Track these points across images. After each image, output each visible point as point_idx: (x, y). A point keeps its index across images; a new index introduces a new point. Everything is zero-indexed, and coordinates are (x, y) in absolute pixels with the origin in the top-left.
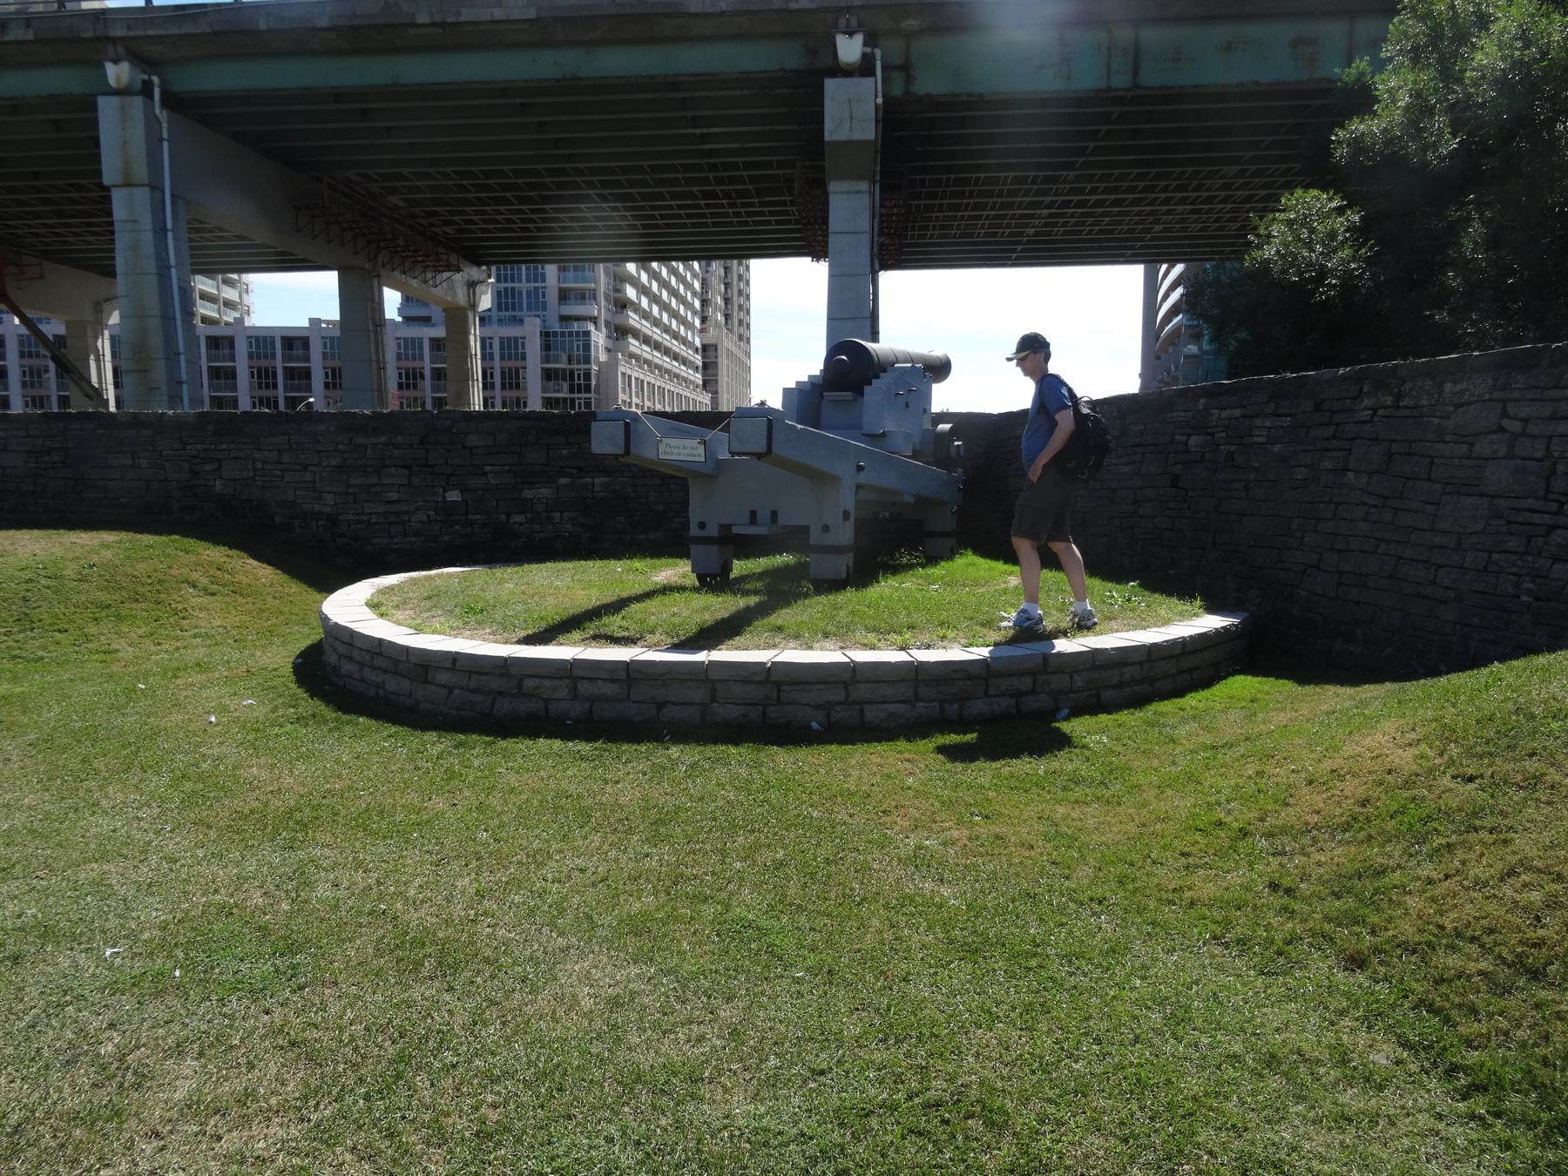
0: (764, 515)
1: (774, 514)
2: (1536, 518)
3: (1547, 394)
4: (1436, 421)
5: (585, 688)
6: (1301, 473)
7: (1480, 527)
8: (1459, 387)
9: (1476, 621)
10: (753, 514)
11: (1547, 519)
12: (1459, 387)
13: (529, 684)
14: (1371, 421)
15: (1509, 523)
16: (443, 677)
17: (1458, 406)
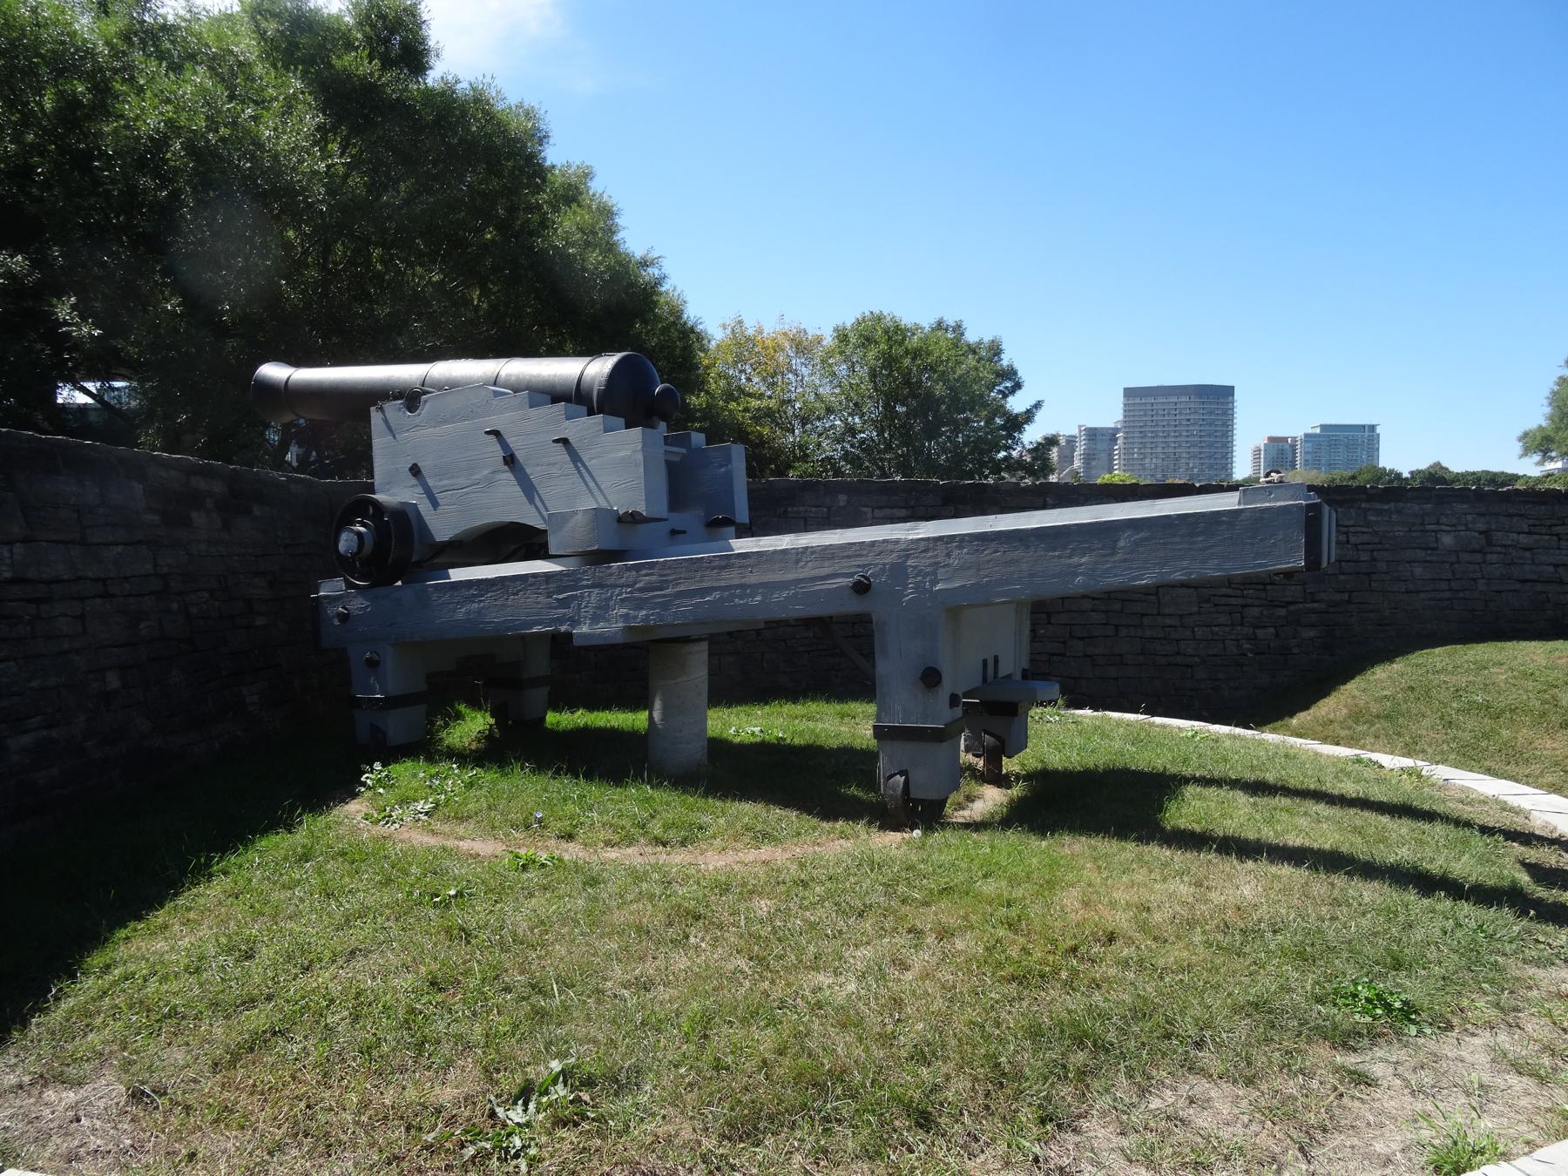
2: (1232, 601)
7: (1195, 609)
11: (1240, 601)
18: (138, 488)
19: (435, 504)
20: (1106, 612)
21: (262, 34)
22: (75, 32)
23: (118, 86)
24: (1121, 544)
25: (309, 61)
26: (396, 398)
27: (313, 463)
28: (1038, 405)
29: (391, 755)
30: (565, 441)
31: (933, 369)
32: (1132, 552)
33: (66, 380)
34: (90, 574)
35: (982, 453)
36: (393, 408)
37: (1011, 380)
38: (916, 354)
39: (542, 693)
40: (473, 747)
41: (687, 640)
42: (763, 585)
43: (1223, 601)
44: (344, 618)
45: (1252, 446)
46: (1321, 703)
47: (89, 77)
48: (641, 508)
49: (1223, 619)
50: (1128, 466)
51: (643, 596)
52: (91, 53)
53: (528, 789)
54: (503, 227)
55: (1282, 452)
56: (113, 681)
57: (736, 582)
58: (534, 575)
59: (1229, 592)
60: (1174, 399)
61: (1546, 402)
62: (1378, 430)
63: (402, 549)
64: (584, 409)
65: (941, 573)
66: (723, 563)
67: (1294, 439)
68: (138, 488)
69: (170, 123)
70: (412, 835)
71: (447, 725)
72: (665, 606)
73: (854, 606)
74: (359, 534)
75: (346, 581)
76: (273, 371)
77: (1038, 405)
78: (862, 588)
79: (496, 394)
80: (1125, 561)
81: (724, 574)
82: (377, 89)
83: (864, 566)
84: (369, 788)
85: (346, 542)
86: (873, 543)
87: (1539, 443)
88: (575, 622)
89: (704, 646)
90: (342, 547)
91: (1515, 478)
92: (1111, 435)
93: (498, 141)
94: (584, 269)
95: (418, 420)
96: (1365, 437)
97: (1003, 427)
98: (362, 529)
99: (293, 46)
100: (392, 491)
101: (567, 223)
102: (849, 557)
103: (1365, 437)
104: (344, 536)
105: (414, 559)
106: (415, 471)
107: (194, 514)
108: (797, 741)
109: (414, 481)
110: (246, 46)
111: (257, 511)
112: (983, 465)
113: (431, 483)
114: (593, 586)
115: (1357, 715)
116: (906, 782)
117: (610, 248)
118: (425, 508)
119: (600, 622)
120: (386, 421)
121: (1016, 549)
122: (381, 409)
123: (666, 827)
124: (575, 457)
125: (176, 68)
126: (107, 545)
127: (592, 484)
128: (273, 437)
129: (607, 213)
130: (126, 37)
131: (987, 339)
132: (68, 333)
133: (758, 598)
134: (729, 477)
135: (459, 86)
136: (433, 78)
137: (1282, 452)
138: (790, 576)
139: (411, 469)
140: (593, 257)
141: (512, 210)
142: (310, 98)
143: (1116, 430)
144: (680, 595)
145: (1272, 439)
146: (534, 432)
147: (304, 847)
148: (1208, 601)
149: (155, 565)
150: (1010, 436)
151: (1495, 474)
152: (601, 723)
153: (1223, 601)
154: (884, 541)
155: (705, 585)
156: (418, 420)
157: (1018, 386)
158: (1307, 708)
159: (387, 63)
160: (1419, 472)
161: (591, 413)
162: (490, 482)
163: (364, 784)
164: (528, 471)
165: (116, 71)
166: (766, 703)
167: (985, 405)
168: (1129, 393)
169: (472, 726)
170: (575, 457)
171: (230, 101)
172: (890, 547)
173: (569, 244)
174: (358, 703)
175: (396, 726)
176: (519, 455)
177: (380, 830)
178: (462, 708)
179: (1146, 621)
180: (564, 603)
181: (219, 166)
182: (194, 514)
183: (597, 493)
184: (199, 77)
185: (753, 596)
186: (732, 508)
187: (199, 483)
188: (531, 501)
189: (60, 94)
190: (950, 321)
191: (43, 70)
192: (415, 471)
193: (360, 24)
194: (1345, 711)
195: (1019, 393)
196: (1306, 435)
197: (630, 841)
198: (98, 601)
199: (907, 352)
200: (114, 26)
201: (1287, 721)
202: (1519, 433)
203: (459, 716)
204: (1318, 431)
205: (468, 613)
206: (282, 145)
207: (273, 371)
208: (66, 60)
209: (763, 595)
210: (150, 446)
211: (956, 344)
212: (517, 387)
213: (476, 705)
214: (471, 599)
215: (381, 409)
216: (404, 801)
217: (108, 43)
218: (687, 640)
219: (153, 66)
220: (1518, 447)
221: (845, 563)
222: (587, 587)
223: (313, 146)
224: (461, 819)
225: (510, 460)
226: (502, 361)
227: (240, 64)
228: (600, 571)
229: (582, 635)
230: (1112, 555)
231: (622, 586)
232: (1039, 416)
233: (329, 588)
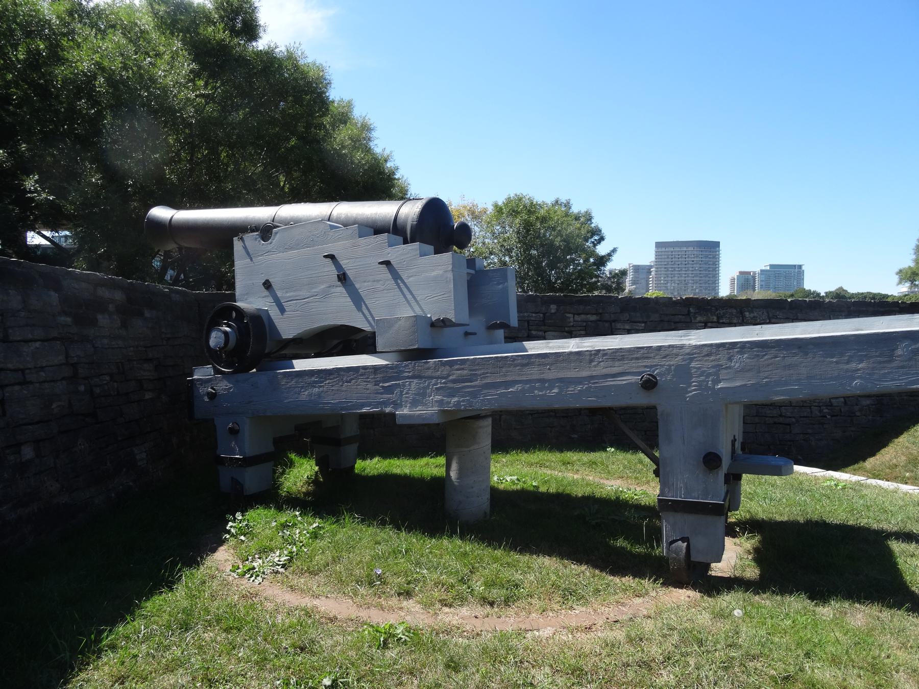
8: (752, 315)
9: (810, 431)
12: (752, 315)
18: (54, 297)
19: (282, 310)
21: (155, 14)
22: (39, 10)
23: (65, 43)
24: (899, 352)
25: (186, 30)
26: (253, 231)
27: (182, 280)
28: (614, 250)
29: (246, 503)
30: (387, 263)
31: (554, 229)
32: (910, 359)
33: (33, 230)
34: (10, 366)
35: (583, 279)
37: (597, 235)
38: (544, 220)
39: (352, 448)
40: (304, 490)
41: (478, 417)
42: (561, 380)
44: (212, 396)
45: (730, 277)
46: (883, 451)
47: (47, 39)
48: (451, 316)
50: (658, 287)
51: (456, 386)
52: (49, 23)
53: (364, 541)
54: (301, 138)
55: (747, 280)
56: (28, 452)
57: (535, 377)
58: (365, 368)
60: (685, 249)
61: (912, 252)
62: (803, 268)
63: (258, 346)
64: (401, 239)
65: (723, 374)
66: (525, 361)
67: (754, 273)
69: (97, 64)
70: (281, 597)
71: (283, 473)
72: (474, 395)
73: (642, 399)
74: (225, 333)
75: (214, 368)
76: (161, 213)
77: (614, 250)
78: (649, 384)
79: (332, 227)
80: (902, 367)
81: (526, 370)
82: (227, 51)
83: (651, 367)
84: (233, 535)
85: (215, 339)
87: (909, 276)
88: (397, 405)
89: (489, 421)
90: (213, 342)
91: (887, 296)
92: (647, 270)
93: (301, 82)
94: (352, 163)
95: (270, 247)
96: (796, 272)
97: (594, 264)
98: (228, 329)
99: (175, 22)
100: (250, 301)
101: (342, 135)
102: (637, 359)
103: (796, 272)
104: (214, 334)
105: (266, 351)
106: (267, 285)
107: (99, 317)
108: (543, 489)
109: (266, 293)
110: (146, 22)
111: (147, 314)
112: (583, 286)
113: (279, 294)
114: (413, 377)
115: (914, 462)
116: (688, 547)
117: (368, 150)
118: (274, 313)
119: (417, 407)
120: (245, 248)
121: (795, 354)
122: (242, 239)
123: (490, 584)
124: (396, 276)
125: (103, 33)
126: (27, 341)
127: (409, 296)
128: (157, 263)
129: (366, 128)
130: (71, 13)
131: (583, 210)
132: (32, 199)
133: (556, 390)
134: (505, 292)
135: (277, 50)
136: (261, 45)
137: (747, 280)
138: (585, 374)
139: (264, 284)
140: (359, 155)
141: (308, 126)
142: (186, 53)
143: (651, 267)
145: (741, 273)
146: (362, 257)
147: (184, 611)
149: (67, 357)
150: (598, 269)
151: (875, 294)
152: (397, 471)
154: (670, 346)
155: (509, 378)
156: (270, 247)
157: (602, 239)
158: (873, 454)
159: (235, 33)
160: (830, 292)
161: (405, 242)
162: (326, 294)
163: (229, 532)
164: (357, 286)
165: (64, 35)
166: (507, 453)
167: (584, 250)
168: (659, 245)
169: (301, 473)
170: (396, 276)
171: (136, 54)
172: (675, 351)
173: (343, 147)
174: (221, 461)
175: (251, 480)
176: (350, 274)
177: (246, 584)
178: (293, 456)
181: (126, 93)
182: (99, 317)
183: (414, 303)
184: (118, 37)
185: (551, 388)
186: (508, 315)
187: (104, 293)
188: (359, 308)
189: (29, 52)
190: (563, 199)
191: (19, 33)
192: (267, 285)
193: (217, 8)
194: (904, 458)
195: (603, 243)
196: (762, 271)
197: (462, 600)
198: (17, 388)
199: (537, 218)
200: (63, 7)
201: (861, 464)
202: (897, 270)
203: (291, 464)
204: (768, 268)
205: (310, 395)
206: (169, 81)
207: (161, 213)
208: (34, 27)
209: (559, 387)
210: (79, 269)
211: (567, 215)
212: (347, 223)
213: (303, 453)
214: (312, 385)
215: (242, 239)
216: (264, 551)
217: (58, 17)
219: (87, 30)
220: (896, 278)
221: (633, 363)
222: (408, 377)
223: (187, 83)
224: (313, 573)
225: (343, 278)
226: (334, 204)
227: (142, 32)
228: (419, 365)
230: (890, 362)
231: (438, 378)
232: (615, 257)
233: (202, 373)
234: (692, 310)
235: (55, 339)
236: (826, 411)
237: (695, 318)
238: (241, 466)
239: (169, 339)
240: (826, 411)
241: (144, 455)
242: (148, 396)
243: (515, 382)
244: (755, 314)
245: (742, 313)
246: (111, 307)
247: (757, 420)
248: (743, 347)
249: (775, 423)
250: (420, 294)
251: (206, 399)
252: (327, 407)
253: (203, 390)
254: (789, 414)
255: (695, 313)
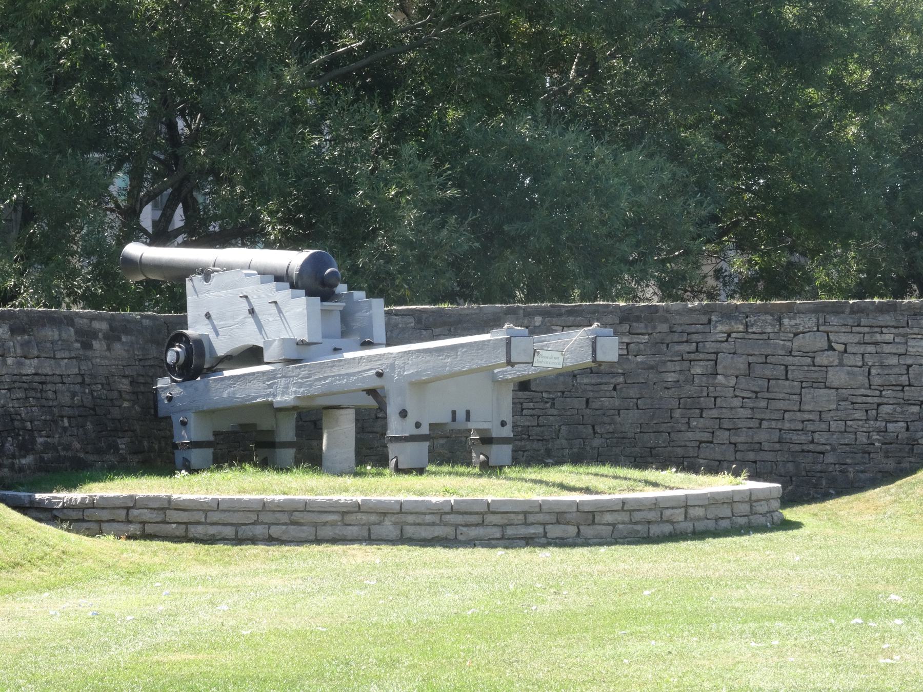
0: (461, 415)
1: (468, 412)
2: (869, 400)
3: (854, 329)
4: (782, 343)
5: (693, 512)
6: (671, 377)
7: (834, 407)
8: (793, 322)
9: (848, 461)
10: (454, 413)
11: (876, 400)
12: (793, 322)
13: (667, 513)
14: (727, 341)
15: (853, 403)
16: (609, 518)
17: (796, 335)
19: (217, 334)
20: (752, 409)
36: (198, 279)
43: (860, 400)
44: (170, 399)
48: (306, 339)
49: (859, 415)
56: (66, 423)
59: (868, 392)
63: (198, 363)
68: (72, 330)
72: (310, 386)
73: (376, 383)
74: (177, 353)
85: (171, 357)
86: (384, 355)
88: (275, 396)
89: (352, 412)
90: (169, 360)
95: (209, 287)
98: (179, 350)
106: (208, 316)
109: (207, 321)
111: (124, 339)
114: (282, 377)
118: (212, 337)
120: (194, 287)
124: (280, 311)
138: (356, 370)
144: (316, 380)
148: (846, 400)
153: (860, 400)
156: (209, 287)
162: (243, 323)
170: (280, 311)
174: (175, 446)
176: (256, 309)
179: (787, 415)
180: (270, 386)
182: (94, 342)
187: (96, 325)
214: (230, 386)
218: (338, 407)
225: (252, 311)
229: (278, 402)
233: (163, 383)
234: (714, 318)
235: (73, 358)
236: (874, 437)
237: (715, 327)
238: (189, 448)
239: (140, 360)
240: (876, 437)
241: (124, 446)
242: (126, 404)
243: (325, 378)
244: (798, 321)
245: (780, 320)
246: (100, 335)
247: (777, 446)
248: (419, 351)
249: (803, 451)
250: (293, 323)
251: (166, 402)
252: (238, 400)
253: (164, 395)
254: (823, 441)
255: (716, 322)
